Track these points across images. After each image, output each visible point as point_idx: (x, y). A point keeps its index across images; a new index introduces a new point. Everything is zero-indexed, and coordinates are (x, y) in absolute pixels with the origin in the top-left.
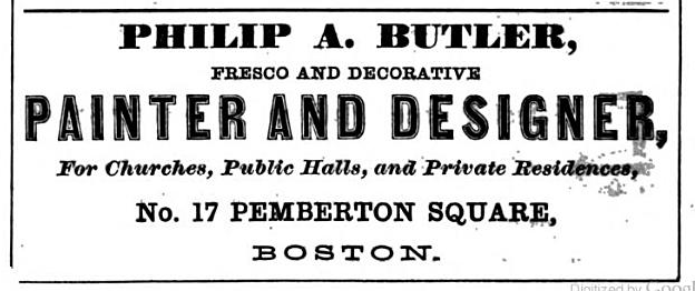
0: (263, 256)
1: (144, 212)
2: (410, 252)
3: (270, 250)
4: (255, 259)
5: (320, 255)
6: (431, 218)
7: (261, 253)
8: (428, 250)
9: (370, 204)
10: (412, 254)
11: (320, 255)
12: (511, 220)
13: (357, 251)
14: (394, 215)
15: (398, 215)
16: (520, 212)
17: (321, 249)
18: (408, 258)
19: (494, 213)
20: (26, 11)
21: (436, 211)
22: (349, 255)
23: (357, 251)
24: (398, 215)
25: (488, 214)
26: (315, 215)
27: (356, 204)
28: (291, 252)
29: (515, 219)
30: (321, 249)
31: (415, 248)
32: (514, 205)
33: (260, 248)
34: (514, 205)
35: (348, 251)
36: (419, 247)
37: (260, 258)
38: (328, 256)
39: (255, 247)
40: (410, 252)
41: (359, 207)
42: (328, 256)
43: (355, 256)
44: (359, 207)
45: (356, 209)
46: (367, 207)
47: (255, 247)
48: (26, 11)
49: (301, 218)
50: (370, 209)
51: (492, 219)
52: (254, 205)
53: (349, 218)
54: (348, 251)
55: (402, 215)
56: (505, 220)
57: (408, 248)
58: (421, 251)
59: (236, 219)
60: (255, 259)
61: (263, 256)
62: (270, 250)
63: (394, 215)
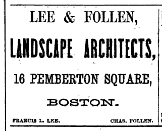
0: (52, 104)
1: (94, 80)
2: (110, 103)
3: (55, 101)
4: (48, 105)
5: (72, 103)
6: (106, 82)
7: (51, 102)
8: (113, 101)
9: (83, 75)
10: (105, 103)
11: (72, 103)
12: (55, 83)
13: (86, 102)
14: (91, 81)
15: (93, 81)
16: (73, 79)
17: (73, 101)
18: (104, 105)
19: (129, 80)
20: (11, 126)
21: (108, 79)
22: (83, 104)
23: (86, 102)
24: (93, 81)
25: (126, 80)
26: (62, 81)
27: (77, 75)
28: (62, 102)
29: (136, 83)
30: (73, 101)
31: (107, 101)
32: (137, 75)
33: (50, 100)
34: (137, 75)
35: (82, 102)
36: (109, 100)
37: (50, 105)
38: (76, 104)
39: (48, 100)
40: (110, 103)
41: (79, 76)
42: (76, 104)
43: (86, 104)
44: (79, 76)
45: (77, 77)
46: (81, 76)
47: (48, 100)
48: (11, 126)
49: (57, 83)
50: (83, 77)
51: (128, 83)
52: (39, 75)
53: (75, 83)
54: (82, 102)
55: (94, 82)
56: (133, 83)
57: (104, 100)
58: (110, 102)
59: (32, 83)
60: (48, 105)
61: (52, 104)
62: (55, 101)
63: (91, 81)
